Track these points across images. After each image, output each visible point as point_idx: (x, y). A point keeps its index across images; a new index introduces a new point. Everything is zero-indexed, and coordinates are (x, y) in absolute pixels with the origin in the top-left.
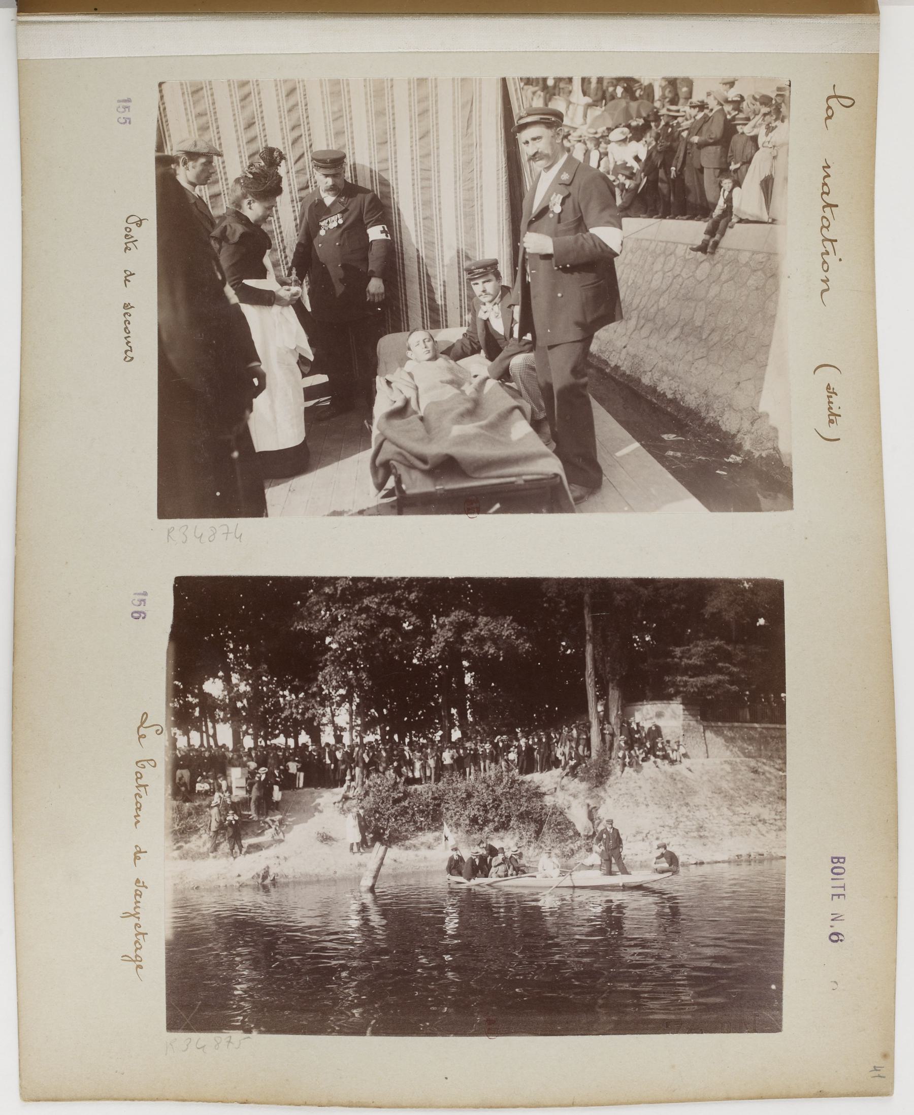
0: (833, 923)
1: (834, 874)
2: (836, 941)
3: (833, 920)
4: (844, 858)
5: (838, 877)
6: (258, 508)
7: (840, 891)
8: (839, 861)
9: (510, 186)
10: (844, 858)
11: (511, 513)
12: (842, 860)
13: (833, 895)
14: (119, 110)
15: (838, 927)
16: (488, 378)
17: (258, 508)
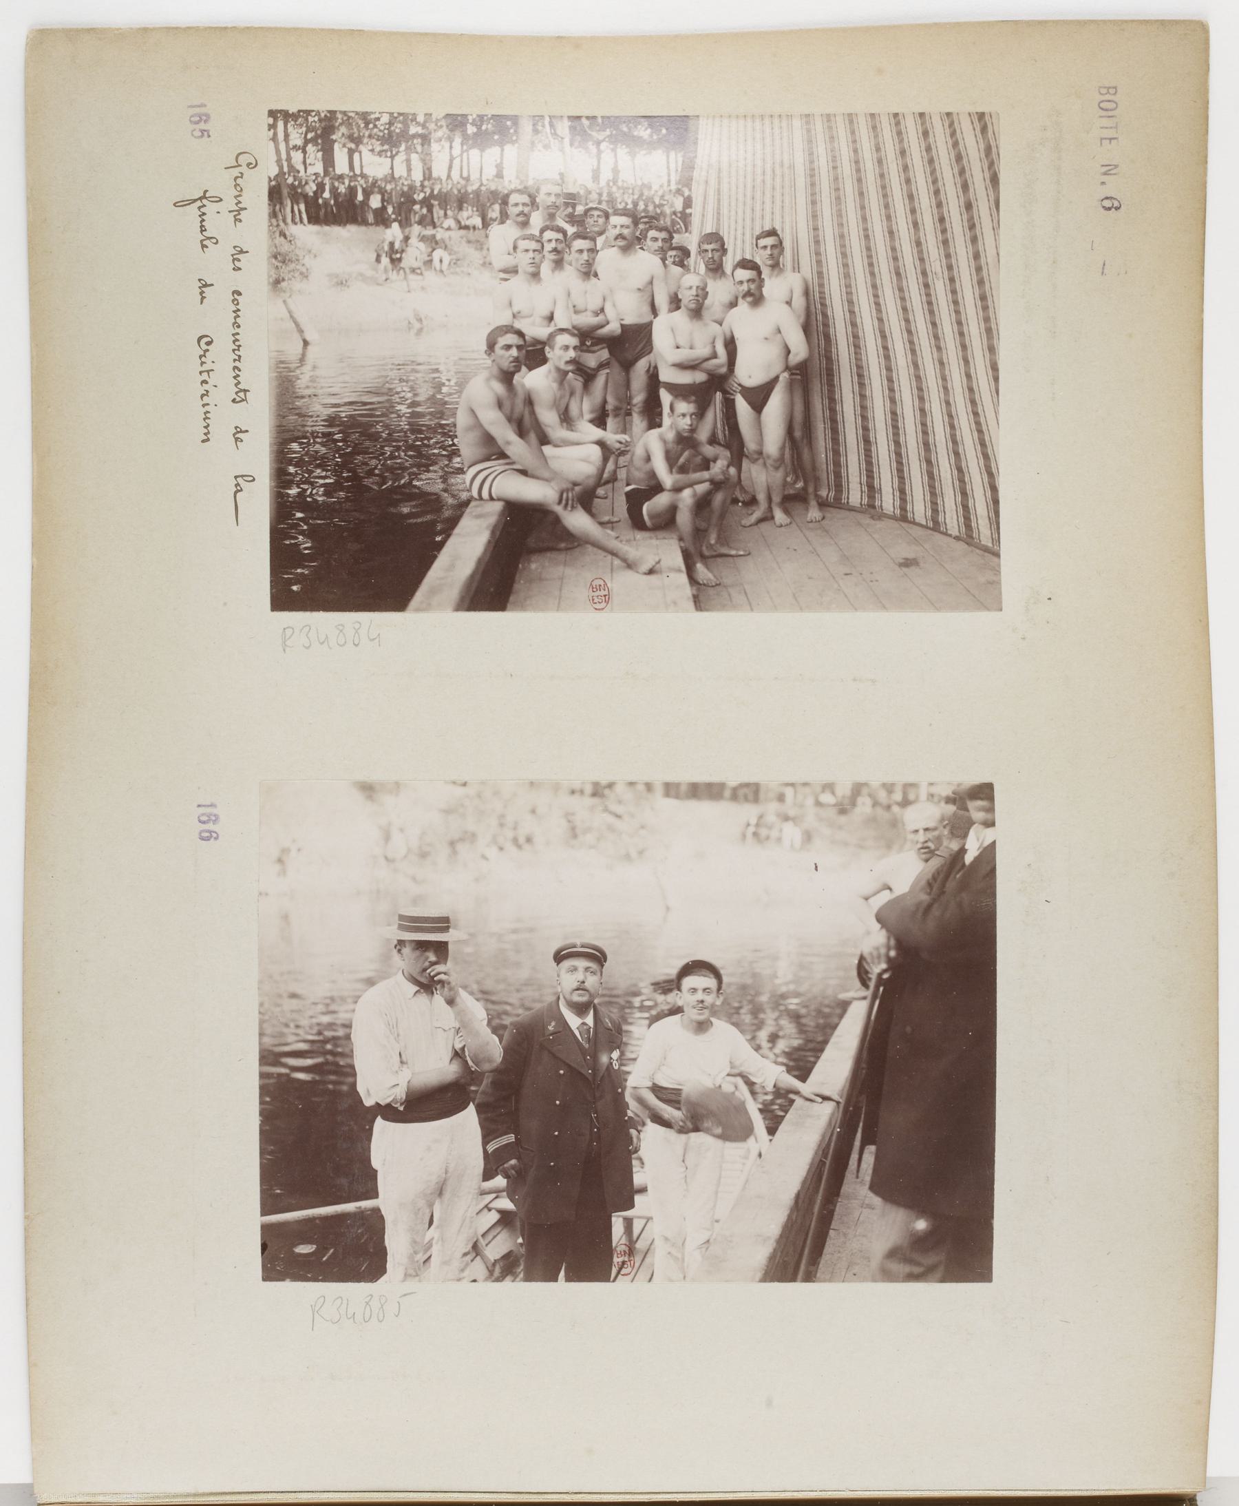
0: (1105, 178)
1: (1102, 109)
2: (1109, 209)
3: (1105, 174)
4: (1115, 88)
5: (1110, 113)
6: (967, 850)
7: (1111, 134)
8: (1108, 93)
9: (304, 1220)
10: (1115, 88)
11: (365, 1281)
12: (1112, 91)
13: (1102, 139)
14: (194, 133)
15: (1113, 187)
16: (389, 1112)
17: (967, 850)
